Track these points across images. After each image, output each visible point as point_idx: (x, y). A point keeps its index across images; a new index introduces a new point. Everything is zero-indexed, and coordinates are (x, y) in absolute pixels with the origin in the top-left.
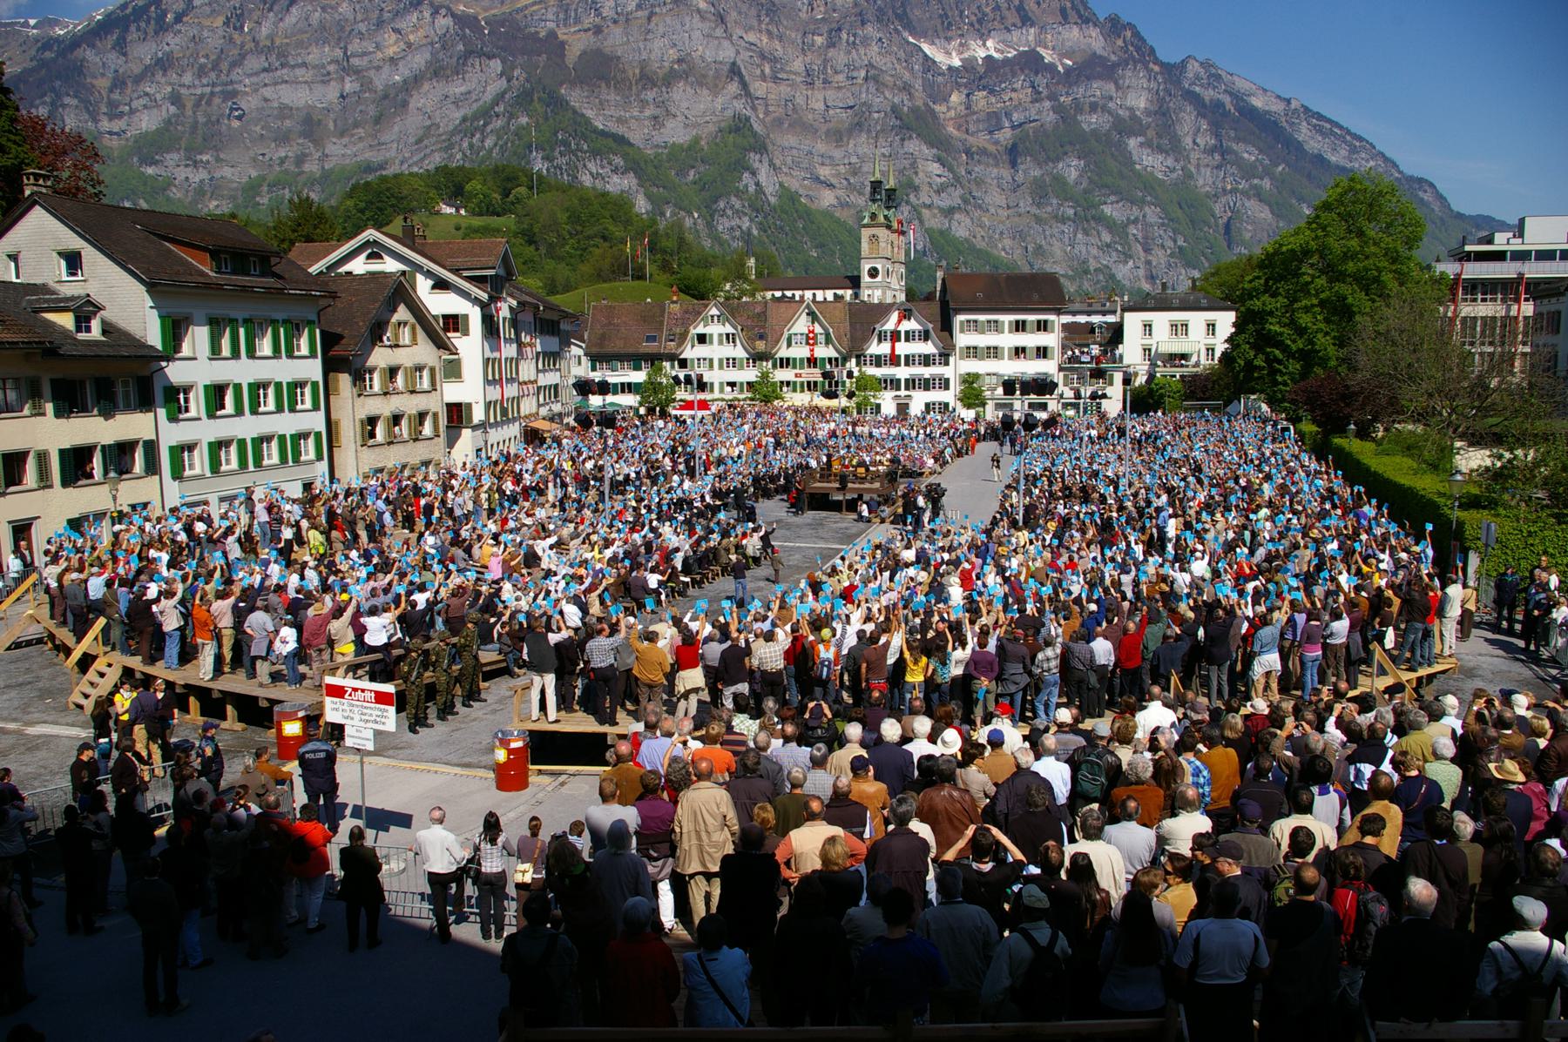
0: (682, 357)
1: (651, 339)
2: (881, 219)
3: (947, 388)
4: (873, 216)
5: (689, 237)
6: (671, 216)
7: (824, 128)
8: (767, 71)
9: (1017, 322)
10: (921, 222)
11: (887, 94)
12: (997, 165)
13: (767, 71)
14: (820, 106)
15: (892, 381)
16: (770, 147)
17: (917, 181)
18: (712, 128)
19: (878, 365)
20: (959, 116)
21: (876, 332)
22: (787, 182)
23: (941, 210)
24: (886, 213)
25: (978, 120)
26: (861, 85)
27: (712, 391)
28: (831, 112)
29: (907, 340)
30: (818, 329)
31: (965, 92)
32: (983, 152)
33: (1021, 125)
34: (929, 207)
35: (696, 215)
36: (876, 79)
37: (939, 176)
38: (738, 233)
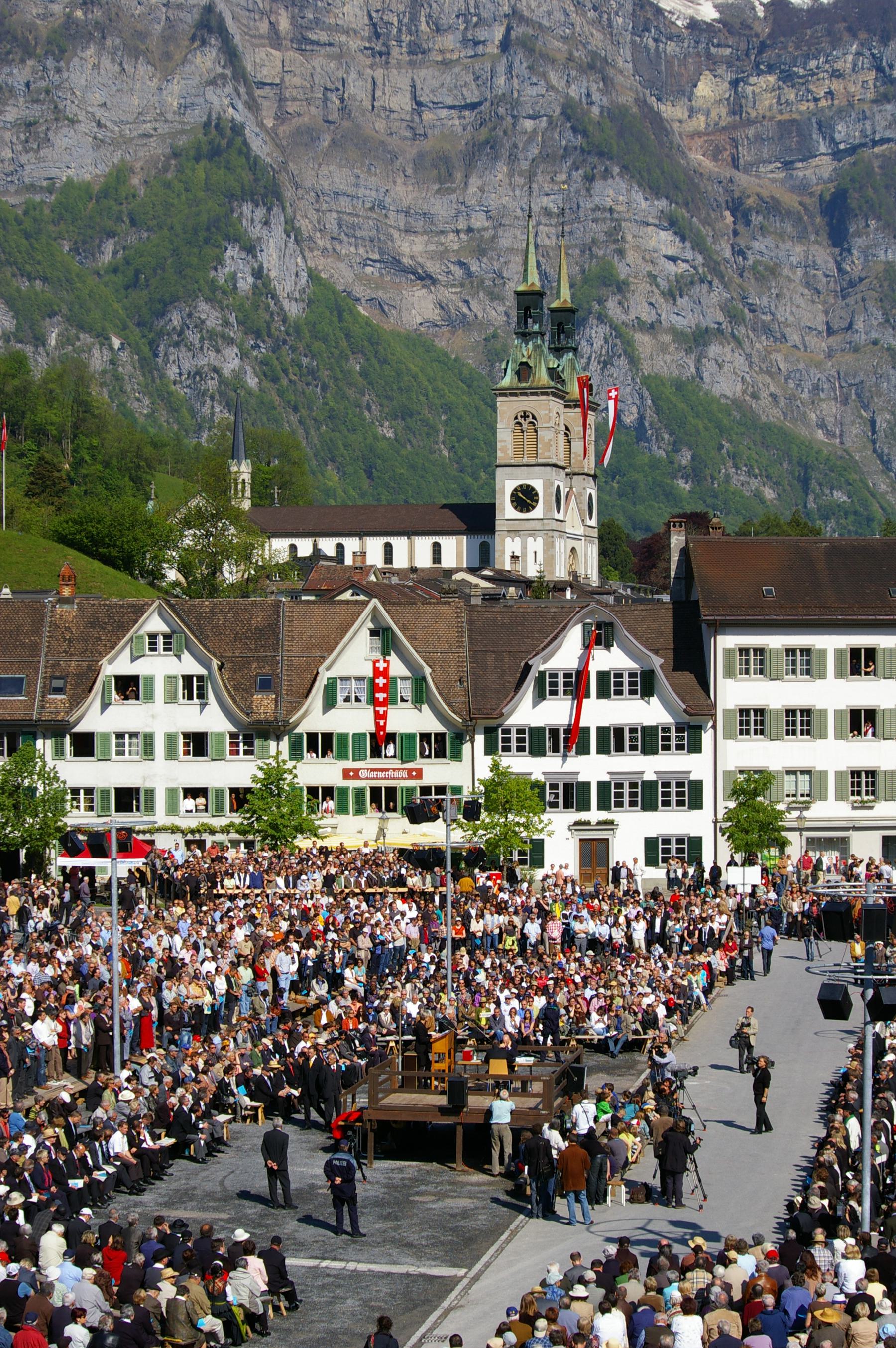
0: (79, 728)
1: (15, 686)
2: (542, 377)
3: (696, 803)
4: (524, 370)
5: (99, 395)
6: (61, 344)
7: (412, 152)
8: (284, 24)
9: (855, 652)
10: (633, 361)
11: (554, 77)
12: (802, 237)
13: (284, 24)
14: (402, 102)
15: (568, 787)
16: (288, 193)
17: (623, 271)
18: (157, 149)
19: (537, 751)
20: (716, 129)
21: (533, 674)
22: (327, 268)
23: (678, 335)
24: (553, 363)
25: (758, 138)
26: (494, 59)
27: (150, 807)
28: (427, 116)
29: (603, 693)
30: (397, 668)
31: (729, 76)
32: (772, 207)
33: (853, 150)
34: (651, 328)
35: (116, 343)
36: (527, 45)
37: (673, 259)
38: (212, 385)
